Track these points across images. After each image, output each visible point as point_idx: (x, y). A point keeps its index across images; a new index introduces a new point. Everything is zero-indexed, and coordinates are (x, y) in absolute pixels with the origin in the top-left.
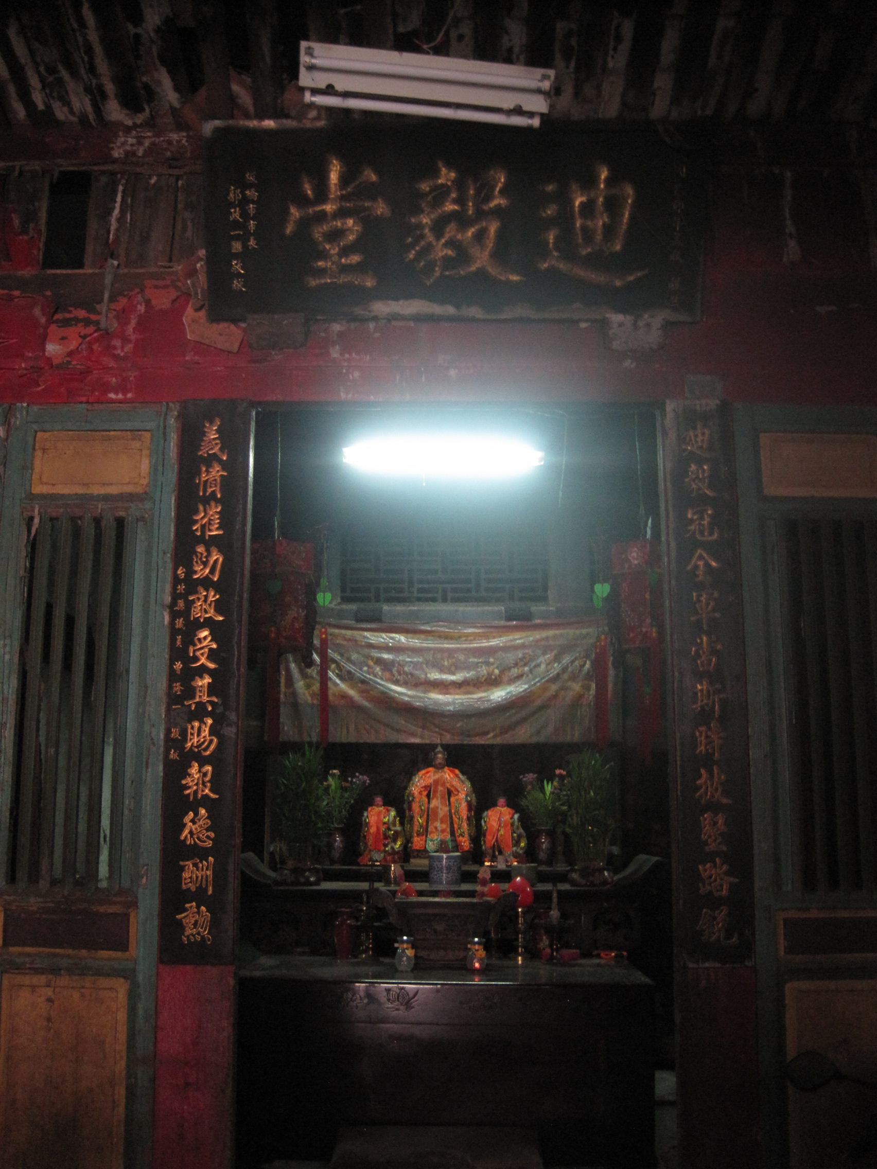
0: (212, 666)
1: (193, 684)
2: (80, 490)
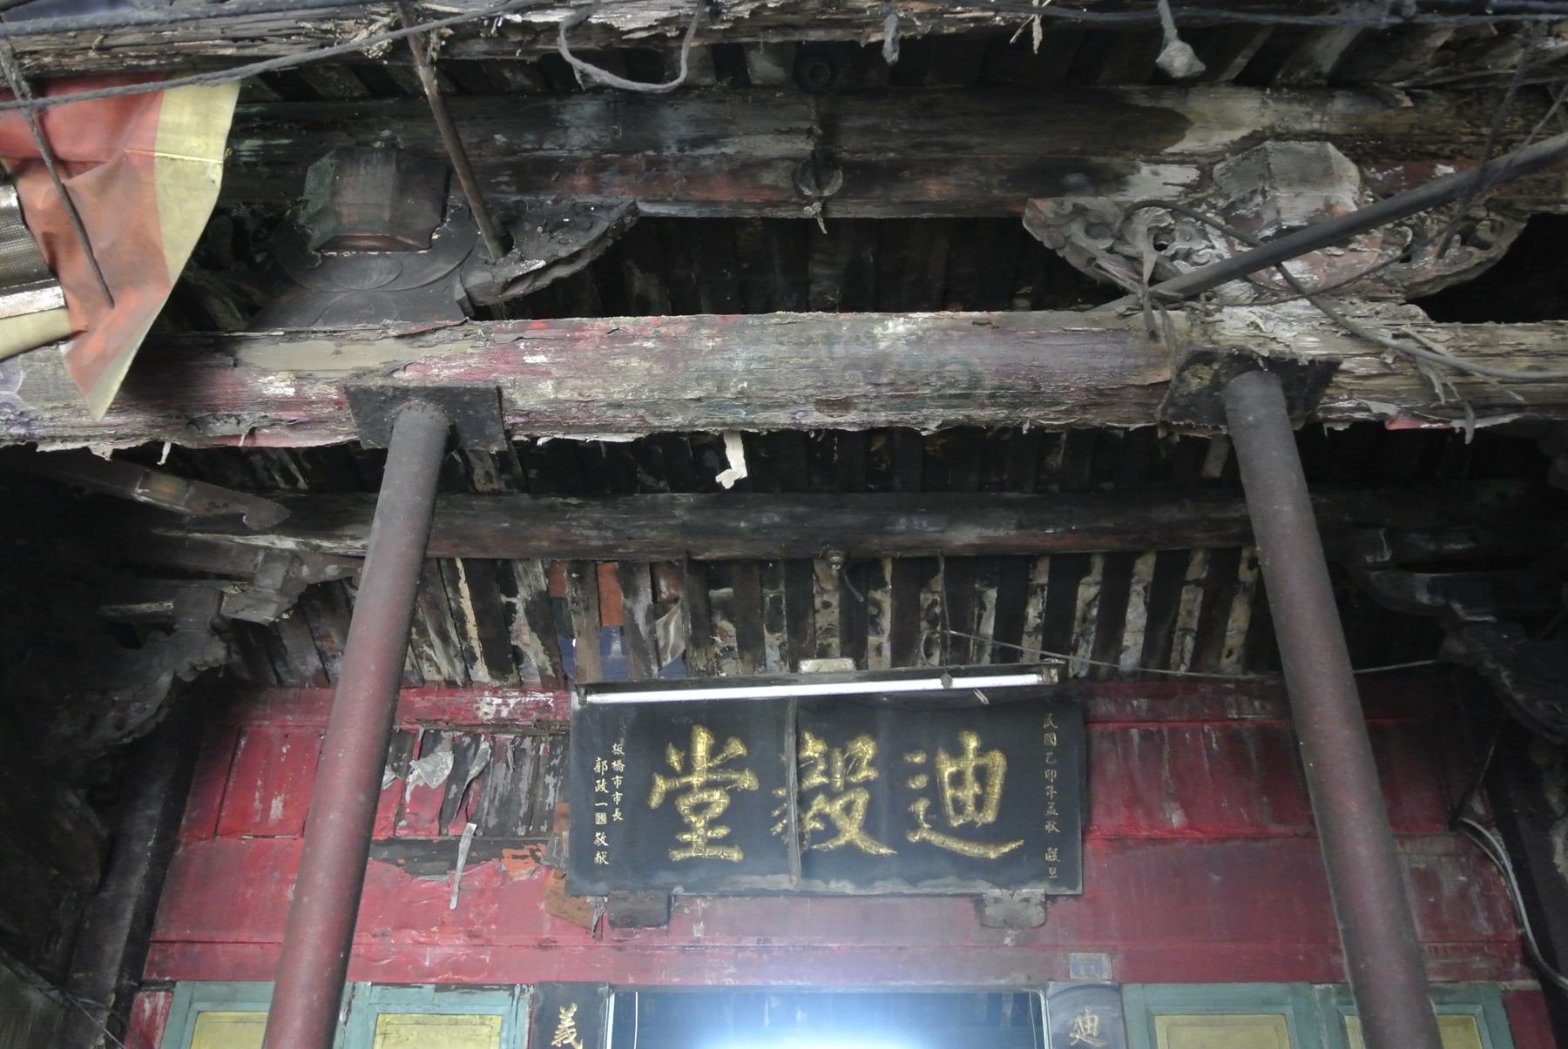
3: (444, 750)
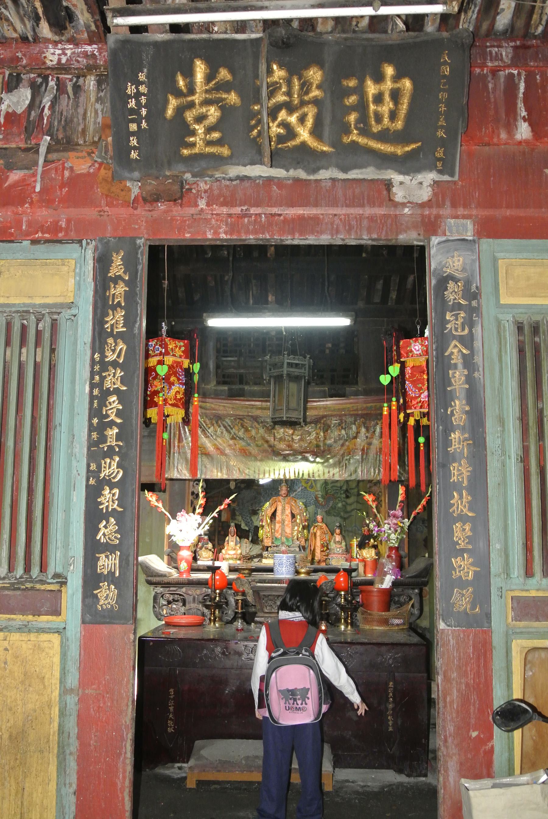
0: (119, 421)
1: (106, 433)
2: (27, 301)
3: (24, 87)
